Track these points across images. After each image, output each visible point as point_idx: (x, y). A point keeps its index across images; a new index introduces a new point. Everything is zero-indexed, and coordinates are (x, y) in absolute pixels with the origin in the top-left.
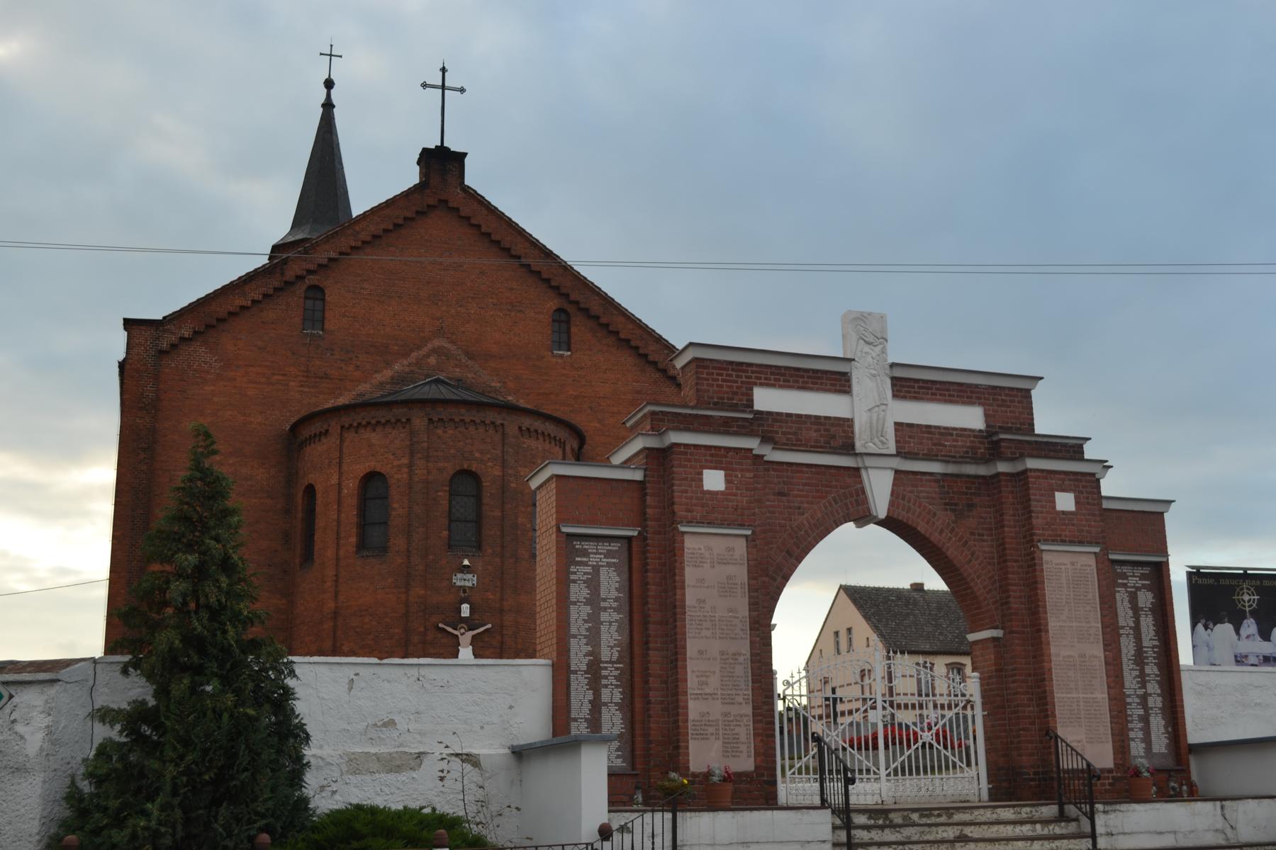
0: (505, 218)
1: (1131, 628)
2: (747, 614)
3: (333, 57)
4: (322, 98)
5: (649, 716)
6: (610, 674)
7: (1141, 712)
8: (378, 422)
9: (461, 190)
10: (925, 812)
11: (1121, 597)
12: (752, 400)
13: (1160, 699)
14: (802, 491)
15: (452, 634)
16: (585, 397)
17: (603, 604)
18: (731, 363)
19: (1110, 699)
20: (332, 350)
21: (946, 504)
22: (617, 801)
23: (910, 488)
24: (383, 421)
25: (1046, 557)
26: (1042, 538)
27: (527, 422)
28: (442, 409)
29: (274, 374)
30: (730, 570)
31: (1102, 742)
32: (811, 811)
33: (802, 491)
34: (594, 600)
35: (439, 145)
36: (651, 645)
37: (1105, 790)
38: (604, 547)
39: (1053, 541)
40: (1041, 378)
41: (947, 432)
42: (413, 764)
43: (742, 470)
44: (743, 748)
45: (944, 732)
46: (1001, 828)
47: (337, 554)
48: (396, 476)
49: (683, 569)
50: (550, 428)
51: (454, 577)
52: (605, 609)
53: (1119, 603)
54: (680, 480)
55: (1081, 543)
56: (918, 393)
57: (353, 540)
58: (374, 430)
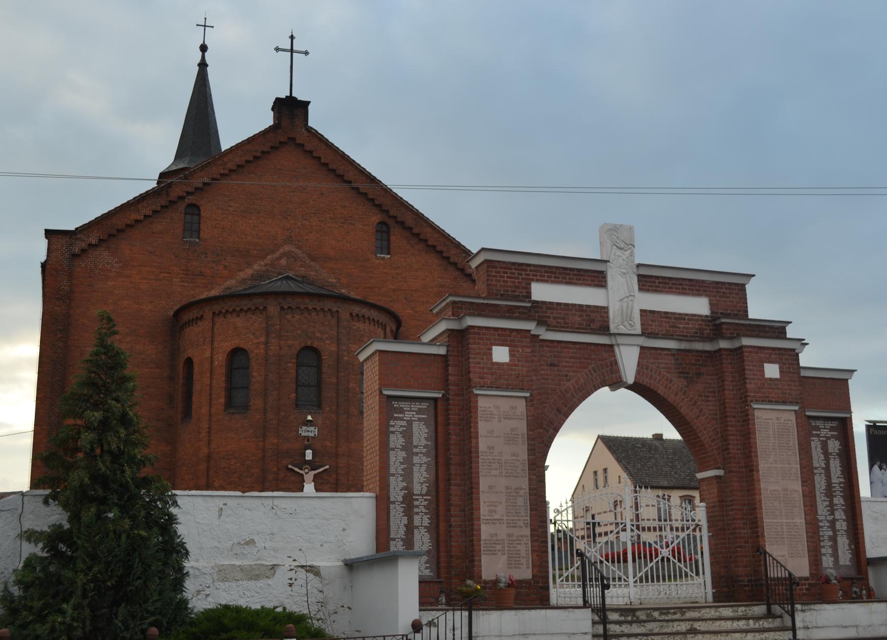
1: (823, 468)
2: (526, 457)
4: (198, 59)
6: (421, 504)
7: (831, 533)
8: (242, 310)
9: (305, 130)
11: (816, 445)
13: (845, 523)
16: (402, 290)
17: (415, 450)
18: (514, 264)
19: (806, 523)
20: (206, 254)
21: (680, 373)
22: (426, 601)
23: (652, 361)
24: (245, 308)
25: (757, 414)
27: (356, 309)
31: (801, 557)
34: (408, 447)
35: (289, 95)
38: (416, 406)
39: (762, 401)
43: (522, 346)
44: (523, 561)
46: (723, 623)
49: (477, 423)
50: (374, 314)
51: (300, 429)
52: (417, 454)
54: (475, 354)
55: (784, 403)
56: (659, 287)
58: (239, 316)
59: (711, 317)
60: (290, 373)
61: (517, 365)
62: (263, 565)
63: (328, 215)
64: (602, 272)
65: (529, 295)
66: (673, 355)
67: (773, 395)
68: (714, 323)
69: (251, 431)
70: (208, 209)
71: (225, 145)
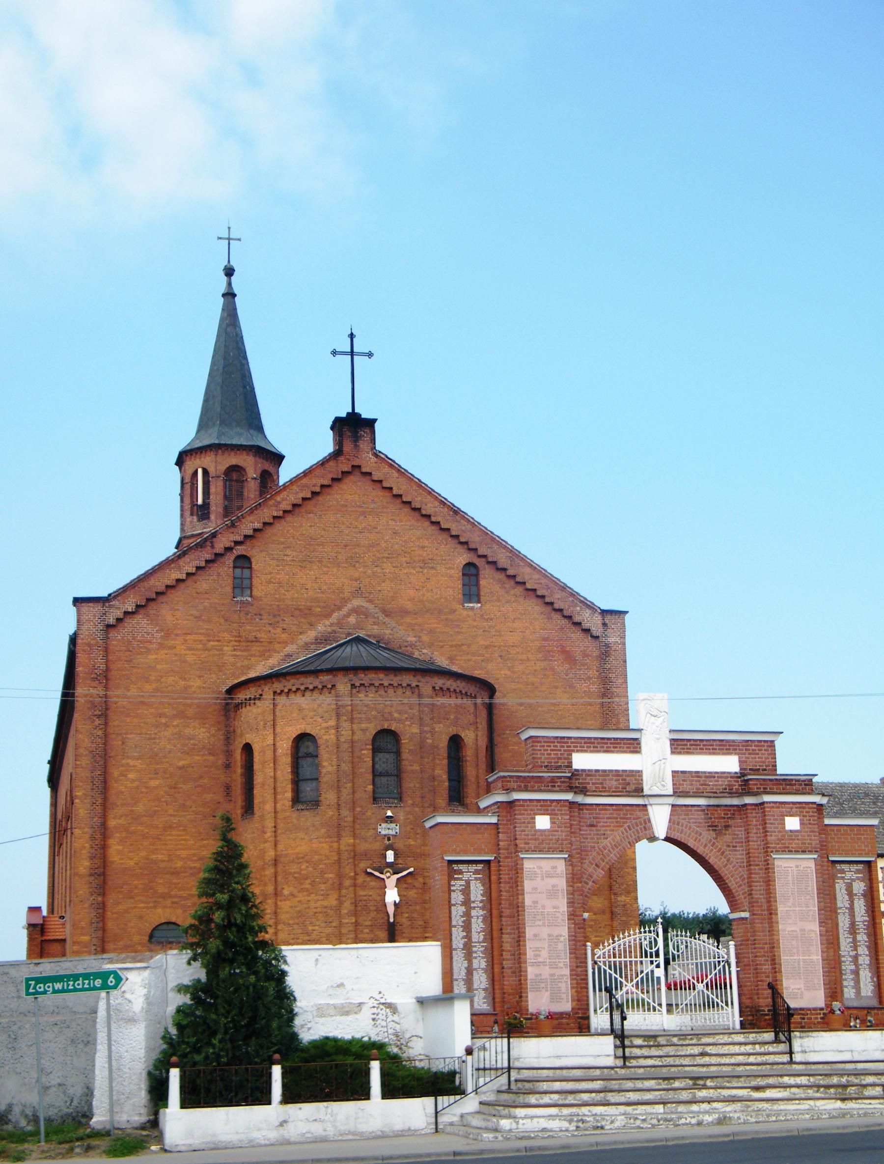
0: (415, 479)
1: (846, 908)
2: (565, 909)
3: (231, 241)
4: (222, 288)
5: (504, 977)
6: (478, 949)
7: (853, 967)
8: (307, 688)
10: (682, 1036)
12: (571, 762)
13: (868, 958)
14: (607, 822)
15: (379, 877)
16: (495, 647)
17: (472, 905)
18: (557, 738)
19: (823, 960)
20: (260, 615)
21: (709, 826)
23: (683, 817)
24: (311, 687)
25: (777, 863)
26: (774, 850)
27: (440, 682)
28: (363, 675)
29: (209, 641)
30: (554, 881)
31: (816, 989)
32: (600, 1037)
33: (607, 822)
34: (467, 902)
35: (350, 411)
36: (503, 931)
37: (818, 1022)
38: (473, 868)
39: (782, 851)
40: (782, 733)
41: (711, 775)
42: (356, 1010)
43: (561, 814)
45: (716, 980)
47: (275, 808)
48: (324, 737)
49: (523, 882)
50: (460, 685)
53: (838, 891)
54: (521, 823)
55: (804, 852)
56: (690, 749)
57: (289, 795)
58: (304, 696)
59: (741, 773)
60: (365, 762)
61: (557, 831)
62: (351, 1003)
63: (404, 559)
64: (636, 739)
65: (570, 765)
66: (704, 810)
67: (794, 845)
68: (742, 778)
69: (323, 831)
70: (260, 560)
71: (281, 483)
